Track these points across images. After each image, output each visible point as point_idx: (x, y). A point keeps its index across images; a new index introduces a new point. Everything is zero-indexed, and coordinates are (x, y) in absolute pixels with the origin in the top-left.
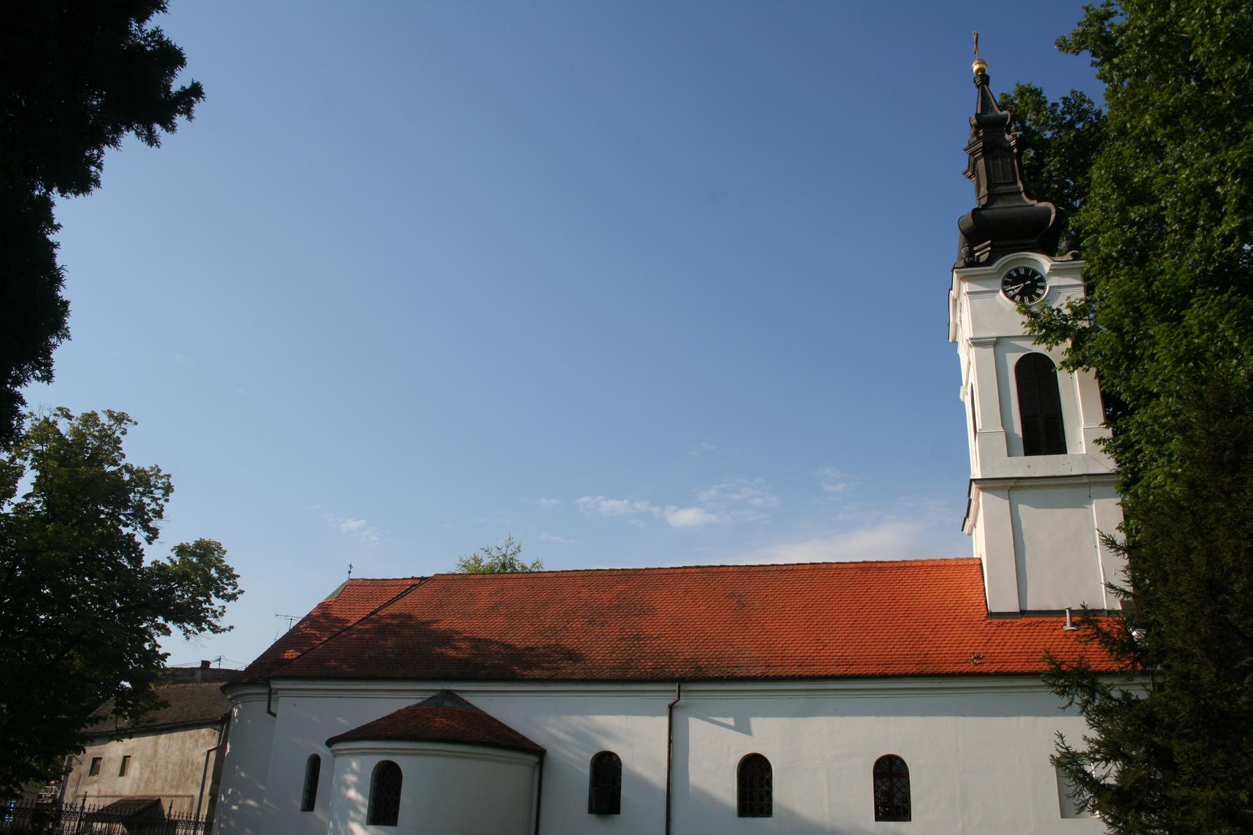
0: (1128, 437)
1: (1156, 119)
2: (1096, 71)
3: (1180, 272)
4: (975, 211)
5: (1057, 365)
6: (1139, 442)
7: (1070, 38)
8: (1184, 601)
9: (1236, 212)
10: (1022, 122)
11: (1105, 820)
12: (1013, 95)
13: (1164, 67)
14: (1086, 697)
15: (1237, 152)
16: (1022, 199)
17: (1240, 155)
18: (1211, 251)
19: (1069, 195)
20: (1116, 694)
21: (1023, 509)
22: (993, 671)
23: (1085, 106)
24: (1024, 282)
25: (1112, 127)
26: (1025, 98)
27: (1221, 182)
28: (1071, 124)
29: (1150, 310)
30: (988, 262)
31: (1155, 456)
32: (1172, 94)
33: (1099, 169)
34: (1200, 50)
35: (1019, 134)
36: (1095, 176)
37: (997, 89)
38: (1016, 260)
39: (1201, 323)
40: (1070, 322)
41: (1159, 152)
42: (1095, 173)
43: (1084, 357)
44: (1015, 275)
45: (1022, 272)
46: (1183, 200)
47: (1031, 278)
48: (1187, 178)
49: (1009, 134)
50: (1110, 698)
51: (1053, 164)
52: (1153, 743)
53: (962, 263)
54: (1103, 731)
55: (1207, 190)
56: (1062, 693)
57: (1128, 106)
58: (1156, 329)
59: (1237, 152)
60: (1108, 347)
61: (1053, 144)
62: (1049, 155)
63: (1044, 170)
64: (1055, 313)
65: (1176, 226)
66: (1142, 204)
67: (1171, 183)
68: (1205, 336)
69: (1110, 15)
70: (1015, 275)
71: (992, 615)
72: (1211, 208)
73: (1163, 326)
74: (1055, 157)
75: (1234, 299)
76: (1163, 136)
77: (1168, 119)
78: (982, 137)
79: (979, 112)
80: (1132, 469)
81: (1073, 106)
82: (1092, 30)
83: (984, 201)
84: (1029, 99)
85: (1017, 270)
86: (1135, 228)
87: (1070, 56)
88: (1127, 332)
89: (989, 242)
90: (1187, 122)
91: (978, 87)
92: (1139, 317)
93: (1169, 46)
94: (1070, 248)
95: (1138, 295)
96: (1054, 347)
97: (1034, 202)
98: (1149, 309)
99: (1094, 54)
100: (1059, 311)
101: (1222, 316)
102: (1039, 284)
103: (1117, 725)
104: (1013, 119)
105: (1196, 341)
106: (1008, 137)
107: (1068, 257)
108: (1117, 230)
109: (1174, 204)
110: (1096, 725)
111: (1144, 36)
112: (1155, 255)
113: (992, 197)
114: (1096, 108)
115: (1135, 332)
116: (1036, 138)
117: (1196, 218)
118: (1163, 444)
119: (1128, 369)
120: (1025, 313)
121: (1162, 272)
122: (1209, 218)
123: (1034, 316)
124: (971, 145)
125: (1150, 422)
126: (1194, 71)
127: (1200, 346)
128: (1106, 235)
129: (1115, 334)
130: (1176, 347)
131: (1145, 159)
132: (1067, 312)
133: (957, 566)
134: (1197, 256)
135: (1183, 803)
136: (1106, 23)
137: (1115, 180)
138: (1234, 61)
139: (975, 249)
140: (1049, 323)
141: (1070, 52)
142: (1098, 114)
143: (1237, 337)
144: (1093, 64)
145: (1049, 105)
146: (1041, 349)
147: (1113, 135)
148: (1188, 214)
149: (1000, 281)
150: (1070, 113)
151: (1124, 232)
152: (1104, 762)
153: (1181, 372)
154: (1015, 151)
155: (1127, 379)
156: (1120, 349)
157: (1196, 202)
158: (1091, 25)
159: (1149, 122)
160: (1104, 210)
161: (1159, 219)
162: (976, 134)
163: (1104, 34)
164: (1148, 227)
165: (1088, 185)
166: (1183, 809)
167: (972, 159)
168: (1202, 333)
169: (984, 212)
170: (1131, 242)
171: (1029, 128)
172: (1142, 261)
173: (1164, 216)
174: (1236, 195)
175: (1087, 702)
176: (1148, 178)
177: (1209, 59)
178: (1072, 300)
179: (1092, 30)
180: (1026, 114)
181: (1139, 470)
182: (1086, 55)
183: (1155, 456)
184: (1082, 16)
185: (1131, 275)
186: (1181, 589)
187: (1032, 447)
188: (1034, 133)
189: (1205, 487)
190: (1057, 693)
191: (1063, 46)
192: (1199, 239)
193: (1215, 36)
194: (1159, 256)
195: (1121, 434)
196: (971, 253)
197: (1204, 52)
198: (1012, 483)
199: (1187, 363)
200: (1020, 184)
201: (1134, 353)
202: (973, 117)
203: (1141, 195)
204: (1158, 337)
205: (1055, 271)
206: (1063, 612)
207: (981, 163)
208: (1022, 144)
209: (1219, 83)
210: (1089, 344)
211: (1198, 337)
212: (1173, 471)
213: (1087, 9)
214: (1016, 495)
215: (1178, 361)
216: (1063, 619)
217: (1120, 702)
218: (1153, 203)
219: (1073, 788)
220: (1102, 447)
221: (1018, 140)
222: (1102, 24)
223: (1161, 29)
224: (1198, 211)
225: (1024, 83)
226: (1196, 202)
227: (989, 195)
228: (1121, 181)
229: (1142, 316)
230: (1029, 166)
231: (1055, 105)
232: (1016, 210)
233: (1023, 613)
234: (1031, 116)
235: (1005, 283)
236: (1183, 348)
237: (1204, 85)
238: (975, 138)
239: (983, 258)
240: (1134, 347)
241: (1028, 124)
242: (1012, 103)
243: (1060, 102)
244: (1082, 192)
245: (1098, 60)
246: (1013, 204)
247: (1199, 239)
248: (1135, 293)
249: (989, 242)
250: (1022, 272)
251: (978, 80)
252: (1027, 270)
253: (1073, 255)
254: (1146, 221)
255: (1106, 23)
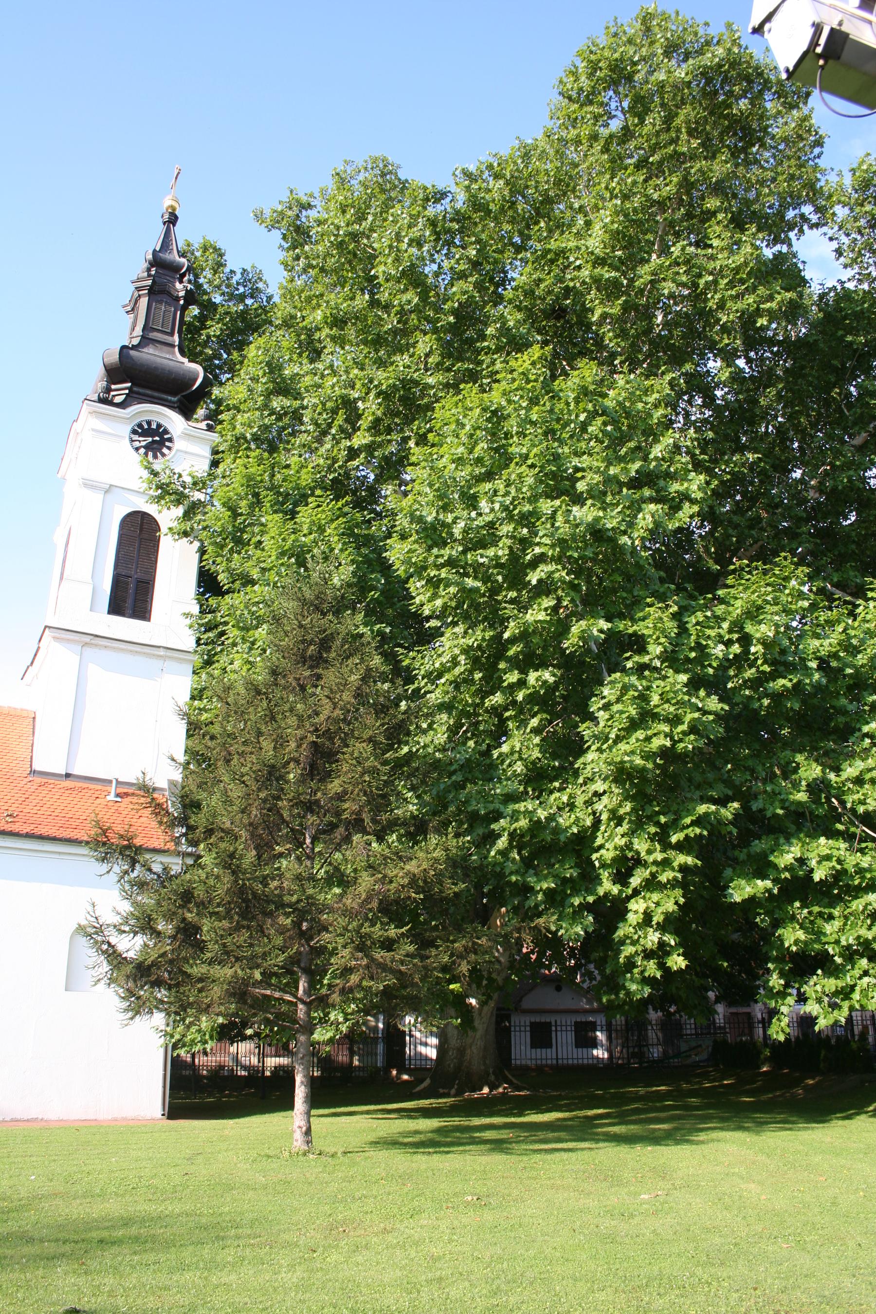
0: (215, 617)
1: (325, 317)
2: (281, 255)
3: (304, 470)
4: (123, 348)
5: (164, 529)
6: (226, 623)
7: (268, 213)
8: (244, 782)
9: (369, 429)
10: (197, 276)
11: (118, 994)
12: (196, 246)
13: (345, 273)
14: (126, 867)
15: (385, 375)
16: (174, 353)
17: (388, 378)
18: (335, 460)
19: (220, 367)
20: (157, 868)
21: (94, 671)
22: (25, 831)
23: (260, 285)
24: (153, 437)
25: (279, 314)
26: (207, 254)
27: (363, 399)
28: (242, 298)
29: (269, 498)
30: (122, 405)
31: (239, 640)
32: (345, 300)
33: (259, 348)
34: (381, 268)
35: (190, 287)
36: (250, 355)
37: (182, 234)
38: (152, 412)
39: (313, 523)
40: (187, 491)
41: (316, 354)
42: (252, 352)
43: (192, 529)
44: (146, 427)
45: (154, 426)
46: (324, 404)
47: (161, 435)
48: (333, 386)
49: (181, 282)
50: (150, 870)
51: (214, 329)
52: (184, 919)
53: (96, 398)
54: (135, 904)
55: (348, 404)
56: (103, 860)
57: (303, 295)
58: (270, 518)
59: (385, 375)
60: (219, 523)
61: (220, 310)
62: (212, 319)
63: (204, 332)
64: (176, 477)
65: (311, 428)
66: (285, 396)
67: (319, 386)
68: (312, 537)
69: (309, 206)
70: (146, 427)
71: (34, 772)
72: (346, 420)
73: (278, 517)
74: (218, 323)
75: (346, 509)
76: (327, 336)
77: (338, 322)
78: (154, 276)
79: (158, 249)
80: (209, 651)
81: (250, 280)
82: (290, 213)
83: (136, 342)
84: (212, 257)
85: (149, 423)
86: (274, 417)
87: (263, 229)
88: (241, 514)
89: (129, 385)
90: (351, 332)
91: (164, 223)
92: (258, 501)
93: (355, 255)
94: (207, 418)
95: (261, 481)
96: (165, 510)
97: (185, 360)
98: (268, 498)
99: (284, 237)
100: (180, 476)
101: (332, 521)
102: (167, 444)
103: (147, 900)
104: (189, 269)
105: (303, 539)
106: (178, 286)
107: (203, 425)
108: (257, 413)
109: (315, 406)
110: (128, 897)
111: (336, 236)
112: (285, 449)
113: (145, 340)
114: (270, 291)
115: (251, 514)
116: (205, 297)
117: (330, 426)
118: (248, 630)
119: (231, 551)
120: (146, 468)
121: (288, 466)
122: (342, 430)
123: (155, 474)
124: (139, 280)
125: (242, 606)
126: (370, 284)
127: (305, 545)
128: (246, 415)
129: (229, 513)
130: (284, 540)
131: (300, 355)
132: (188, 480)
133: (8, 714)
134: (321, 461)
135: (201, 980)
136: (304, 213)
137: (269, 364)
138: (406, 290)
139: (113, 387)
140: (168, 485)
141: (264, 225)
142: (269, 298)
143: (340, 546)
144: (281, 246)
145: (227, 270)
146: (152, 509)
147: (278, 322)
148: (325, 420)
149: (129, 429)
150: (245, 286)
151: (262, 417)
152: (132, 935)
153: (282, 564)
154: (182, 302)
155: (229, 560)
156: (230, 529)
157: (334, 411)
158: (290, 208)
159: (319, 318)
160: (250, 390)
161: (297, 416)
162: (149, 270)
163: (299, 223)
164: (286, 420)
165: (242, 363)
166: (200, 986)
167: (136, 295)
168: (310, 534)
169: (133, 353)
170: (266, 428)
171: (201, 285)
172: (273, 449)
173: (302, 415)
174: (373, 413)
175: (126, 872)
176: (298, 374)
177: (387, 280)
178: (194, 469)
179: (290, 213)
180: (203, 270)
181: (216, 654)
182: (277, 235)
183: (239, 640)
184: (285, 197)
185: (260, 461)
186: (244, 770)
187: (116, 607)
188: (205, 293)
189: (284, 676)
190: (97, 860)
191: (259, 217)
192: (328, 446)
193: (397, 260)
194: (289, 450)
195: (210, 612)
196: (108, 390)
197: (384, 272)
198: (87, 639)
199: (289, 558)
200: (176, 337)
201: (241, 537)
202: (151, 252)
203: (284, 388)
204: (270, 525)
205: (187, 436)
206: (110, 782)
207: (144, 301)
208: (191, 298)
209: (387, 307)
210: (199, 517)
211: (304, 535)
212: (251, 659)
213: (291, 191)
214: (89, 652)
215: (283, 554)
216: (108, 788)
217: (159, 876)
218: (296, 399)
219: (94, 959)
220: (188, 621)
221: (189, 293)
222: (300, 211)
223: (354, 236)
224: (334, 420)
225: (212, 238)
226: (334, 411)
227: (142, 337)
228: (273, 367)
229: (259, 503)
230: (190, 324)
231: (232, 272)
232: (166, 362)
233: (68, 775)
234: (208, 273)
235: (134, 432)
236: (290, 542)
237: (374, 303)
238: (146, 274)
239: (118, 399)
240: (243, 531)
241: (201, 281)
242: (193, 254)
243: (239, 272)
244: (232, 368)
245: (286, 245)
246: (164, 355)
247: (328, 446)
248: (259, 478)
249: (129, 385)
250: (154, 426)
251: (166, 216)
252: (159, 426)
253: (208, 425)
254: (286, 414)
255: (304, 213)
